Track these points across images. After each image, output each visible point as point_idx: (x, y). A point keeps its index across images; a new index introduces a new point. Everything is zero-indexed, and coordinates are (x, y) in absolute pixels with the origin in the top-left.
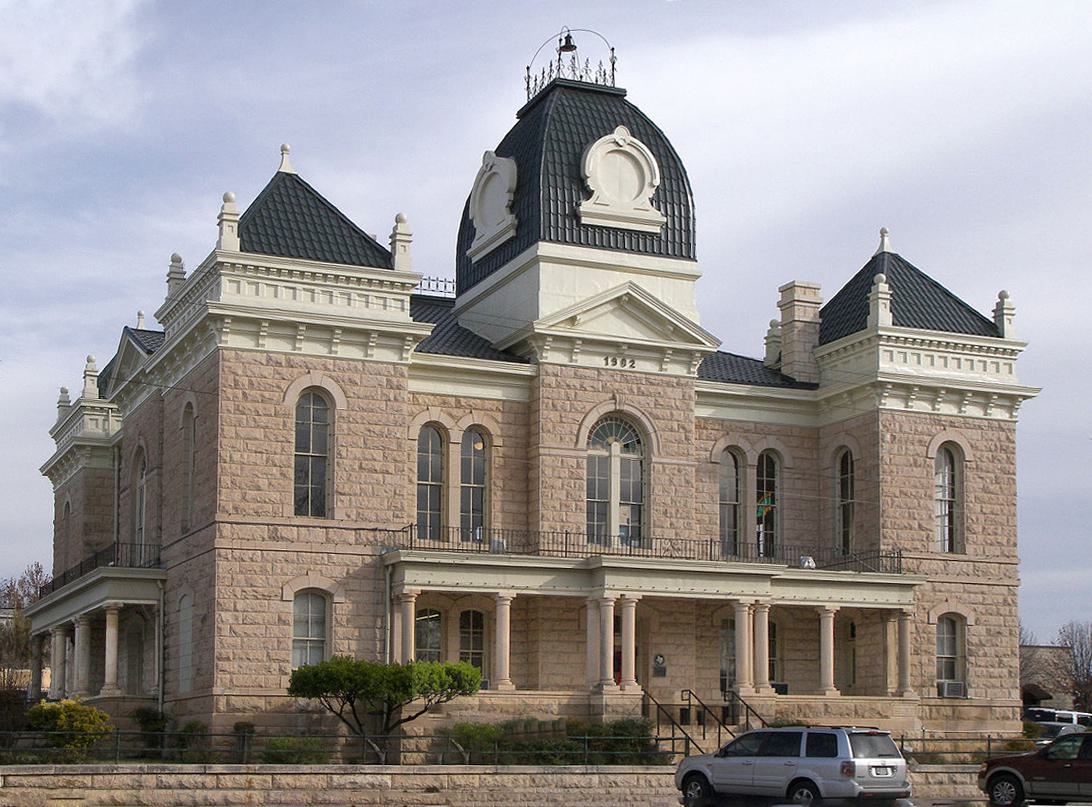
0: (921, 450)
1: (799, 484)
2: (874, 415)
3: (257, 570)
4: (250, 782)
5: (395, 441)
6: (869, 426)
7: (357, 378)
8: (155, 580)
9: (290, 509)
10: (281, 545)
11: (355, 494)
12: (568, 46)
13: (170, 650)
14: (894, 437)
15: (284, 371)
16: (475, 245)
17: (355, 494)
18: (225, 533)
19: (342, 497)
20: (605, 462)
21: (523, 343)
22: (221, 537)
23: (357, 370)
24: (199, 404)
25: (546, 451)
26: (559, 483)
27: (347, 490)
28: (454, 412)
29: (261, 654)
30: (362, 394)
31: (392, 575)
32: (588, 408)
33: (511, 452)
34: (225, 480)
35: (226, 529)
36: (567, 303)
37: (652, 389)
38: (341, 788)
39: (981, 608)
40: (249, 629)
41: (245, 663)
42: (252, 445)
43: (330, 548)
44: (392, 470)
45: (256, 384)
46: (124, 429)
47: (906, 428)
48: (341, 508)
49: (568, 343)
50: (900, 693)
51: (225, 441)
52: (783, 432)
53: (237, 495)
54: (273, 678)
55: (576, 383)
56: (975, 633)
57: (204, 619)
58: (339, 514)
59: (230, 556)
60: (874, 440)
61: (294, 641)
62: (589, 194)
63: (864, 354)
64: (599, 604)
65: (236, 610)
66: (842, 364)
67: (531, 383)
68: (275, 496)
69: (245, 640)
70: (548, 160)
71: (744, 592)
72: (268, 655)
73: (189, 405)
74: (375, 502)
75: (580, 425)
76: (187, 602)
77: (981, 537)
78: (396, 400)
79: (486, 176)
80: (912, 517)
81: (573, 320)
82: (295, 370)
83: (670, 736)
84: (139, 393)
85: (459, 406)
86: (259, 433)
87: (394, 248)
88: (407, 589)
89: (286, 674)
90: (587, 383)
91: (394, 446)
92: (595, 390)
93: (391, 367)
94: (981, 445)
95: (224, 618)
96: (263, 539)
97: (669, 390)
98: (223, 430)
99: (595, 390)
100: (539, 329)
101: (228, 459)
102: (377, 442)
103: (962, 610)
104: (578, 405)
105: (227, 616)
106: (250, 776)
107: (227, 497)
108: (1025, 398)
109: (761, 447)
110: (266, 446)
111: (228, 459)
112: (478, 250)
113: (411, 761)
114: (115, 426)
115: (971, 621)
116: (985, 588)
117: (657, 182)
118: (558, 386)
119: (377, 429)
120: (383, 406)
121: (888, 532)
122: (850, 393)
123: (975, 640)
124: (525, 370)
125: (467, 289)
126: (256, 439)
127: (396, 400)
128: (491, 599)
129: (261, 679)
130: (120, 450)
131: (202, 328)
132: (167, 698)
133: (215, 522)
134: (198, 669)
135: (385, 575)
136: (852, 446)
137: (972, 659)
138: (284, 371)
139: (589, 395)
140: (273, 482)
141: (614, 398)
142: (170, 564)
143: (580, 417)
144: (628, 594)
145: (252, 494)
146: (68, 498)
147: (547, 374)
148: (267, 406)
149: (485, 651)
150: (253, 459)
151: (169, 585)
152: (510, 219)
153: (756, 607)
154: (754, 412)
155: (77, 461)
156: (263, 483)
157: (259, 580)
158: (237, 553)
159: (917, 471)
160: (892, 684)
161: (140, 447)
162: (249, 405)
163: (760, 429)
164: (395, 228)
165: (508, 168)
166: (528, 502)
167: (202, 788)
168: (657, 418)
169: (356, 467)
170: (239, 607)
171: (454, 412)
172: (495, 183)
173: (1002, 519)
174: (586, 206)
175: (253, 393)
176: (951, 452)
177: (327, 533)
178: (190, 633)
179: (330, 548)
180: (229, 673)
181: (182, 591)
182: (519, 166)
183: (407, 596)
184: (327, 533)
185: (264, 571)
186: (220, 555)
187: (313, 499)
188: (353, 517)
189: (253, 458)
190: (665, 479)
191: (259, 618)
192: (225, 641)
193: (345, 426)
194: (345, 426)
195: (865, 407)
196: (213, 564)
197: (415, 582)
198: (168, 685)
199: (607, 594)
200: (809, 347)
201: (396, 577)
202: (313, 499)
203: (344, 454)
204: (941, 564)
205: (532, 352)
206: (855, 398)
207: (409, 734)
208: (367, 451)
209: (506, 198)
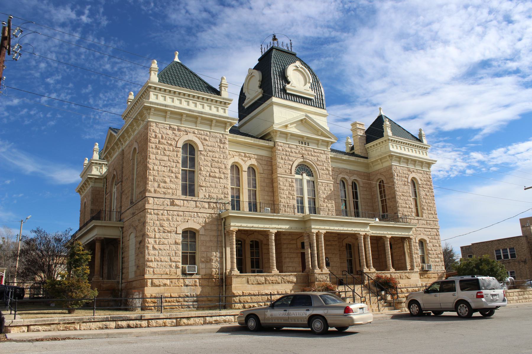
0: (406, 180)
1: (365, 193)
2: (390, 167)
3: (165, 219)
4: (165, 323)
5: (223, 165)
6: (389, 173)
7: (207, 138)
8: (119, 227)
9: (180, 192)
10: (176, 208)
11: (208, 187)
12: (275, 39)
13: (125, 259)
14: (397, 175)
15: (176, 132)
16: (246, 102)
17: (208, 187)
18: (150, 202)
19: (202, 188)
20: (301, 180)
21: (269, 134)
22: (148, 203)
23: (207, 135)
24: (139, 147)
25: (280, 175)
26: (285, 188)
27: (204, 185)
28: (244, 158)
29: (167, 259)
30: (210, 145)
31: (224, 223)
32: (294, 160)
33: (266, 176)
34: (151, 178)
35: (151, 200)
36: (283, 120)
37: (316, 154)
38: (210, 323)
39: (430, 237)
40: (162, 247)
41: (160, 263)
42: (163, 163)
43: (197, 210)
44: (223, 177)
45: (164, 137)
46: (108, 170)
47: (401, 172)
48: (202, 194)
49: (285, 135)
50: (412, 269)
51: (151, 161)
52: (359, 174)
53: (156, 184)
54: (173, 270)
55: (289, 150)
56: (430, 246)
57: (140, 242)
58: (201, 195)
59: (152, 213)
60: (391, 176)
61: (182, 253)
62: (289, 83)
63: (379, 148)
64: (309, 235)
65: (155, 238)
66: (376, 149)
67: (272, 149)
68: (173, 186)
69: (160, 252)
70: (274, 70)
71: (362, 231)
72: (170, 259)
73: (135, 148)
74: (216, 190)
75: (292, 166)
76: (133, 236)
77: (427, 211)
78: (223, 148)
79: (250, 76)
80: (406, 204)
81: (286, 126)
82: (182, 133)
83: (272, 297)
84: (114, 153)
85: (245, 156)
86: (166, 158)
87: (221, 89)
88: (232, 229)
89: (179, 268)
90: (293, 150)
91: (223, 167)
92: (296, 153)
93: (196, 214)
94: (423, 179)
95: (150, 242)
96: (168, 205)
97: (321, 155)
98: (149, 156)
99: (296, 153)
100: (276, 127)
101: (152, 169)
102: (217, 165)
103: (425, 238)
104: (291, 158)
105: (151, 241)
106: (165, 320)
107: (151, 186)
108: (433, 163)
109: (353, 178)
110: (168, 164)
111: (152, 169)
112: (247, 104)
113: (237, 307)
114: (104, 170)
115: (428, 242)
116: (430, 230)
117: (311, 81)
118: (283, 150)
119: (216, 159)
120: (218, 150)
121: (400, 209)
122: (381, 159)
123: (430, 249)
124: (271, 144)
125: (243, 118)
126: (164, 161)
127: (223, 148)
128: (265, 234)
129: (167, 270)
130: (106, 179)
131: (141, 114)
132: (123, 281)
133: (146, 197)
134: (138, 267)
135: (221, 223)
136: (383, 178)
137: (430, 256)
138: (176, 132)
139: (294, 155)
140: (172, 180)
141: (303, 156)
142: (125, 220)
143: (291, 163)
144: (321, 231)
145: (162, 185)
146: (85, 200)
147: (278, 145)
148: (170, 147)
149: (260, 257)
150: (163, 169)
151: (124, 229)
152: (260, 90)
153: (365, 236)
154: (350, 165)
155: (89, 184)
156: (168, 180)
157: (166, 224)
158: (156, 211)
159: (406, 187)
160: (409, 267)
161: (114, 175)
162: (161, 146)
163: (351, 173)
164: (221, 82)
165: (258, 75)
166: (273, 196)
167: (140, 327)
168: (318, 165)
169: (208, 175)
170: (157, 236)
171: (244, 158)
172: (253, 79)
173: (431, 205)
174: (288, 86)
175: (163, 141)
176: (414, 182)
177: (196, 204)
178: (134, 250)
179: (197, 210)
180: (152, 268)
181: (132, 230)
182: (262, 73)
183: (233, 231)
184: (196, 204)
185: (168, 220)
186: (148, 212)
187: (189, 189)
188: (207, 197)
189: (163, 169)
190: (323, 188)
191: (166, 242)
192: (151, 254)
193: (203, 158)
194: (203, 158)
195: (386, 164)
196: (145, 217)
197: (235, 226)
198: (124, 275)
199: (313, 231)
200: (363, 144)
201: (227, 223)
202: (189, 189)
203: (203, 169)
204: (417, 221)
205: (272, 138)
206: (383, 161)
207: (236, 294)
208: (212, 169)
209: (258, 84)
